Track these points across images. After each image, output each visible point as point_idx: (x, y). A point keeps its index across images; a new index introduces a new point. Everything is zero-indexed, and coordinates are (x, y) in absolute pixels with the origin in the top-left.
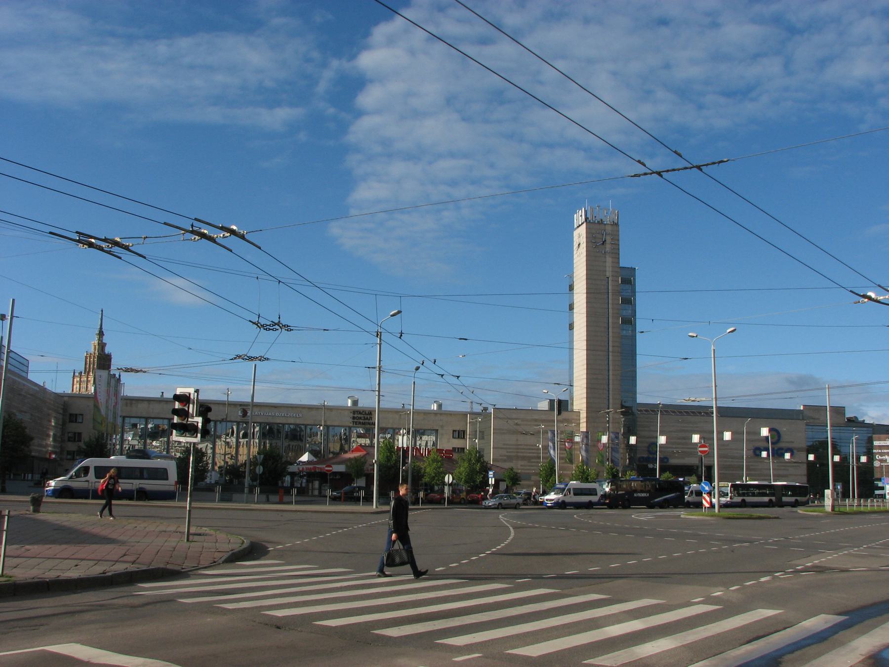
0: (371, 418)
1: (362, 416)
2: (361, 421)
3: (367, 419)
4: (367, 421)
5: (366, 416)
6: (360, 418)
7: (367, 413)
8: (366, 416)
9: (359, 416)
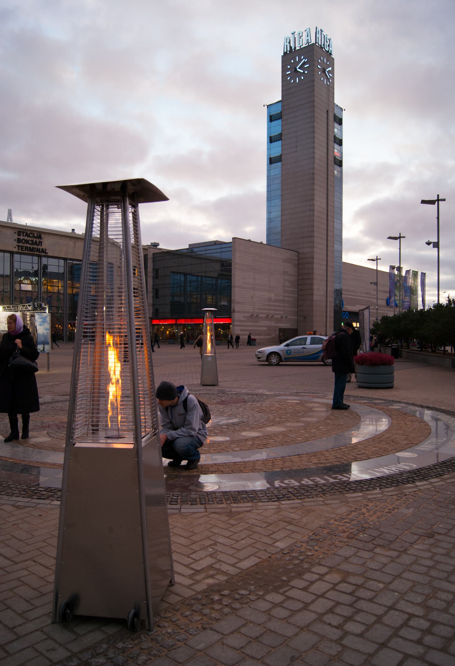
0: (41, 242)
1: (29, 239)
2: (29, 246)
3: (36, 243)
4: (35, 246)
5: (35, 240)
6: (27, 242)
7: (36, 235)
8: (35, 240)
9: (26, 238)
